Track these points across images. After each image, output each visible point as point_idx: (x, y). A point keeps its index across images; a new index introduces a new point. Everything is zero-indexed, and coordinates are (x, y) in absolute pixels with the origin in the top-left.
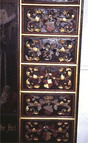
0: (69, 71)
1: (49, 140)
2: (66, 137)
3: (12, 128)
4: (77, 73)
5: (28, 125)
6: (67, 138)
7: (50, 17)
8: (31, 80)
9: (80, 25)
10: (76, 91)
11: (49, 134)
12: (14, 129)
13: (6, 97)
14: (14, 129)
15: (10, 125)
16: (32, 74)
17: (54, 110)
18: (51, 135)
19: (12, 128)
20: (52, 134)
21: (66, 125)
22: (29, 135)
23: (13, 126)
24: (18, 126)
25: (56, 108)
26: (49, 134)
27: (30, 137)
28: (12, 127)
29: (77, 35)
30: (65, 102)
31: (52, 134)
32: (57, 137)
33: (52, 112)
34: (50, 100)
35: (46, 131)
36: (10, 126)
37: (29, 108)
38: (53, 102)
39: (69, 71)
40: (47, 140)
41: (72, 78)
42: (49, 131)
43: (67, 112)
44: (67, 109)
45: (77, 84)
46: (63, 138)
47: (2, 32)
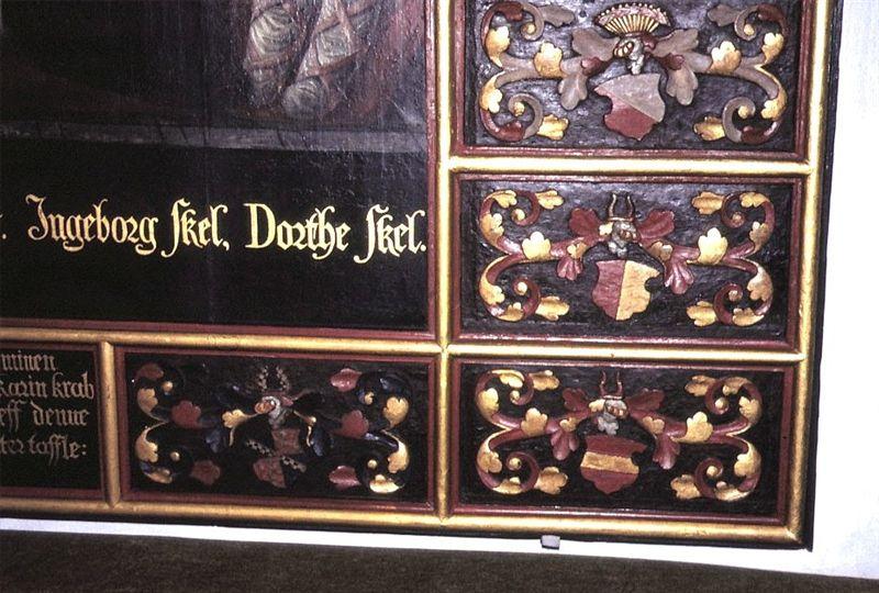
0: (743, 392)
1: (635, 315)
2: (754, 297)
3: (392, 236)
4: (797, 492)
5: (495, 207)
6: (755, 305)
7: (626, 50)
8: (509, 274)
9: (826, 68)
10: (795, 520)
11: (637, 274)
12: (404, 240)
13: (350, 17)
14: (404, 240)
15: (377, 216)
16: (514, 230)
17: (672, 105)
18: (651, 285)
19: (393, 233)
20: (654, 272)
21: (753, 214)
22: (509, 274)
23: (399, 219)
24: (432, 221)
25: (683, 85)
26: (637, 274)
27: (511, 296)
28: (394, 224)
29: (794, 347)
30: (747, 48)
31: (654, 272)
32: (690, 298)
33: (659, 117)
34: (644, 34)
35: (615, 256)
36: (381, 222)
37: (498, 447)
38: (664, 49)
39: (743, 392)
40: (623, 314)
41: (781, 260)
42: (637, 252)
43: (757, 120)
44: (758, 95)
45: (806, 409)
46: (729, 306)
47: (312, 446)
